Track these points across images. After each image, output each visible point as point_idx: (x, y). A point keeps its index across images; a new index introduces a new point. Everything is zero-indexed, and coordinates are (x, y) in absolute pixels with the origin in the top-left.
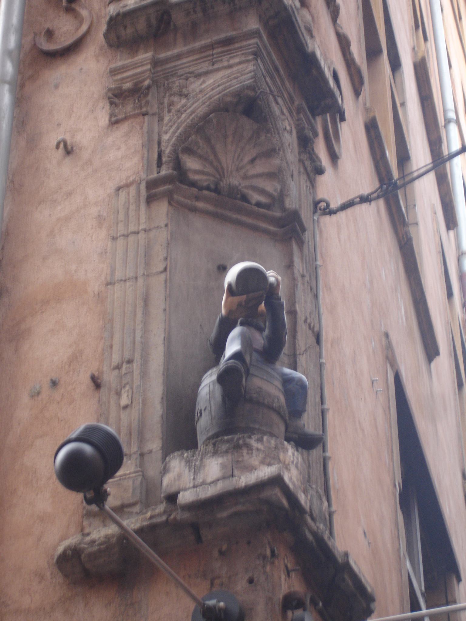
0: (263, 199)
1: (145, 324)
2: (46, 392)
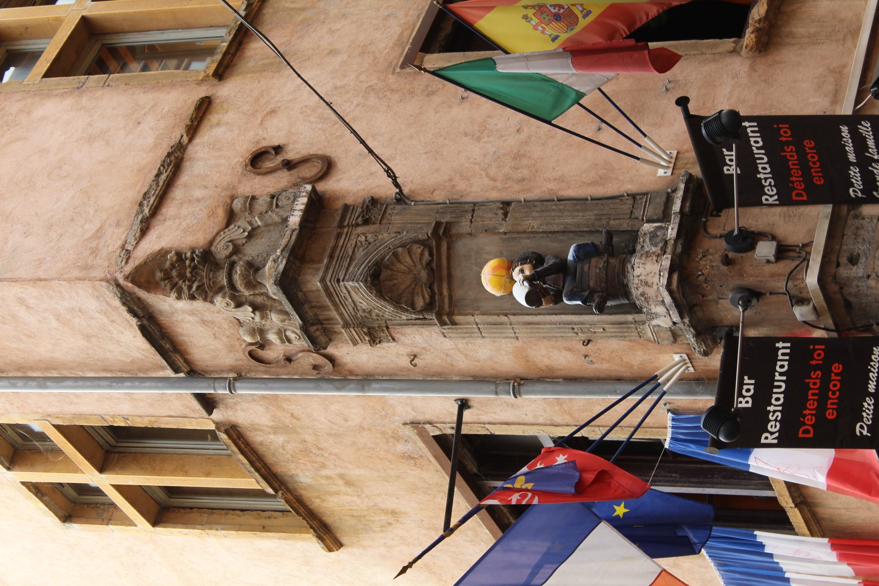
0: (426, 253)
1: (545, 324)
2: (590, 359)
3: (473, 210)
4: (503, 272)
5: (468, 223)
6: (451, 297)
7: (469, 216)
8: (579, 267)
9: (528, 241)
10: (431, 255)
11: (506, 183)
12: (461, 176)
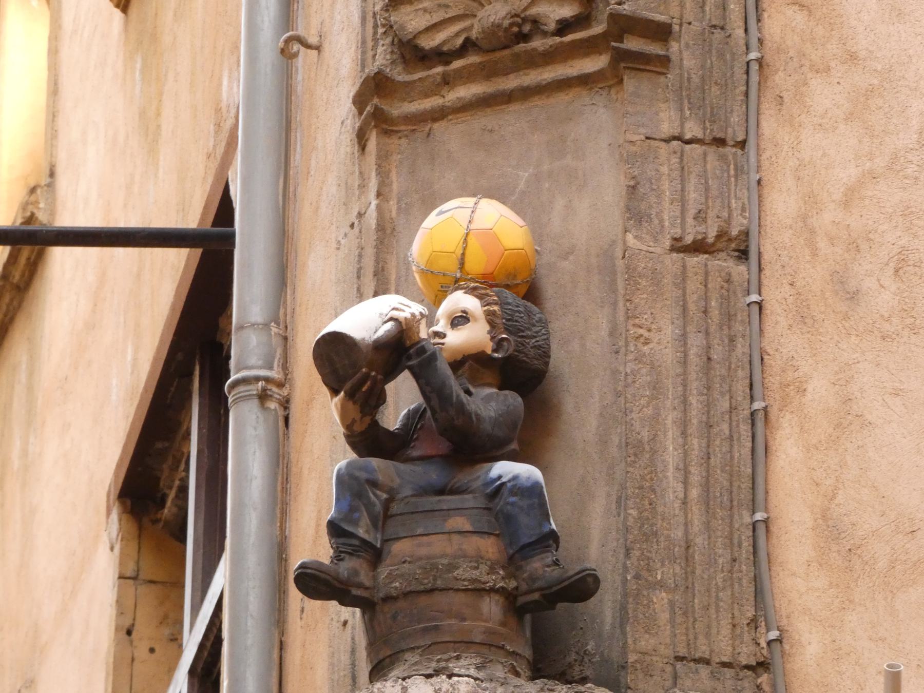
3: (720, 142)
4: (477, 263)
5: (667, 128)
6: (439, 114)
7: (692, 130)
8: (468, 500)
9: (604, 333)
10: (564, 27)
11: (832, 240)
12: (870, 92)
